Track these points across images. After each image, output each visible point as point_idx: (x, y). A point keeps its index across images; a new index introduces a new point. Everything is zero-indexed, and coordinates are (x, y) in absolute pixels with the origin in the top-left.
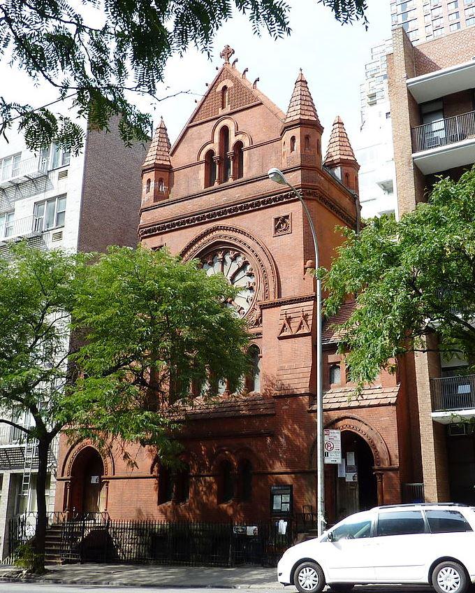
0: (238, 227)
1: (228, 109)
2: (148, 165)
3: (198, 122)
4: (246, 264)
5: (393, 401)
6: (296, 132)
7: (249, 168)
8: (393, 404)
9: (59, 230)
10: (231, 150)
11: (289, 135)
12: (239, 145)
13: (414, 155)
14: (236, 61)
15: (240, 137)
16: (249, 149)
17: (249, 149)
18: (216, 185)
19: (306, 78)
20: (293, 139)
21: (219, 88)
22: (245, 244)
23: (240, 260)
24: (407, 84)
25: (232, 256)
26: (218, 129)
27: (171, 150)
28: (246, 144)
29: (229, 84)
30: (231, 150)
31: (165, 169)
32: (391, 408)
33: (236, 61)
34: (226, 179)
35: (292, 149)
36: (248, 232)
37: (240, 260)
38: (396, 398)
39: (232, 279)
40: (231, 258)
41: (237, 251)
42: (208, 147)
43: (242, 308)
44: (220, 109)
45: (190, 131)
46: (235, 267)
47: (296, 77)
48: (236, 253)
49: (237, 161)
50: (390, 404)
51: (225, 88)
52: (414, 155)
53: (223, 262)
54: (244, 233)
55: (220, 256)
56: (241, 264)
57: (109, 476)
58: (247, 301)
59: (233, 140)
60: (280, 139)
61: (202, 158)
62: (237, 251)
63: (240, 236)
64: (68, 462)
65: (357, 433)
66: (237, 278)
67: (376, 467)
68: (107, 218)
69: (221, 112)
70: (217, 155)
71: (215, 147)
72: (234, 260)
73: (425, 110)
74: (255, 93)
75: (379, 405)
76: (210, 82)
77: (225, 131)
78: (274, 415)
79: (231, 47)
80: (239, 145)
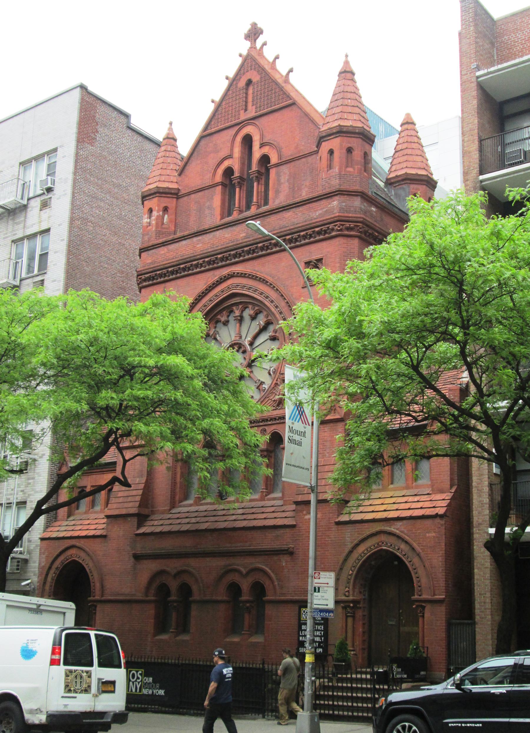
0: (259, 274)
1: (252, 112)
2: (397, 176)
3: (213, 130)
4: (268, 324)
5: (441, 511)
6: (335, 143)
7: (277, 192)
8: (441, 516)
9: (40, 278)
10: (255, 167)
11: (326, 146)
12: (265, 159)
13: (481, 177)
14: (265, 44)
15: (266, 150)
16: (277, 165)
17: (277, 165)
18: (235, 215)
19: (354, 67)
20: (331, 152)
21: (242, 83)
22: (267, 297)
23: (261, 320)
24: (478, 77)
25: (252, 312)
26: (239, 139)
27: (264, 208)
28: (274, 160)
29: (256, 78)
30: (255, 167)
31: (171, 194)
32: (438, 520)
33: (265, 44)
34: (248, 208)
35: (330, 167)
36: (270, 279)
37: (261, 320)
38: (445, 508)
39: (251, 344)
40: (250, 315)
41: (258, 306)
42: (226, 164)
43: (262, 383)
44: (242, 112)
45: (203, 142)
46: (255, 327)
47: (339, 67)
48: (256, 308)
49: (263, 181)
50: (437, 516)
51: (249, 83)
52: (481, 177)
53: (240, 320)
54: (264, 281)
55: (237, 313)
56: (262, 323)
57: (97, 598)
58: (270, 374)
59: (257, 154)
60: (317, 152)
61: (219, 178)
62: (258, 306)
63: (262, 287)
64: (49, 579)
65: (395, 552)
66: (258, 342)
67: (416, 597)
68: (103, 259)
69: (243, 116)
70: (237, 174)
71: (235, 164)
72: (253, 318)
73: (509, 110)
74: (287, 88)
75: (423, 517)
76: (231, 75)
77: (248, 141)
78: (293, 526)
79: (259, 26)
80: (265, 159)
